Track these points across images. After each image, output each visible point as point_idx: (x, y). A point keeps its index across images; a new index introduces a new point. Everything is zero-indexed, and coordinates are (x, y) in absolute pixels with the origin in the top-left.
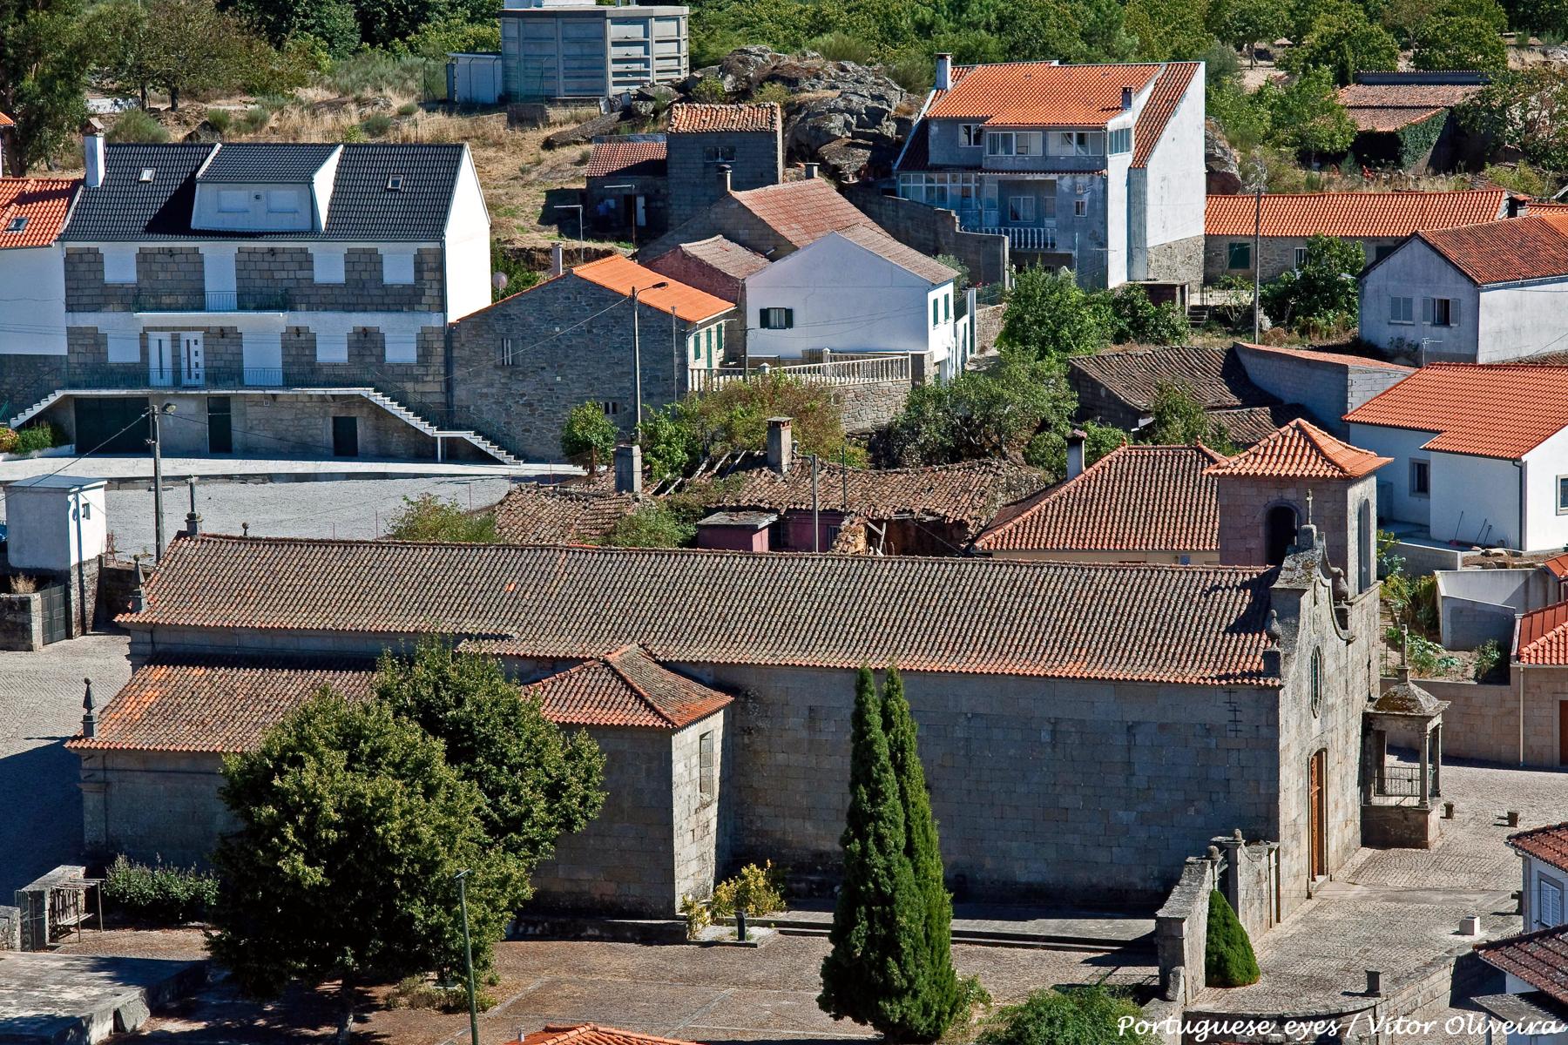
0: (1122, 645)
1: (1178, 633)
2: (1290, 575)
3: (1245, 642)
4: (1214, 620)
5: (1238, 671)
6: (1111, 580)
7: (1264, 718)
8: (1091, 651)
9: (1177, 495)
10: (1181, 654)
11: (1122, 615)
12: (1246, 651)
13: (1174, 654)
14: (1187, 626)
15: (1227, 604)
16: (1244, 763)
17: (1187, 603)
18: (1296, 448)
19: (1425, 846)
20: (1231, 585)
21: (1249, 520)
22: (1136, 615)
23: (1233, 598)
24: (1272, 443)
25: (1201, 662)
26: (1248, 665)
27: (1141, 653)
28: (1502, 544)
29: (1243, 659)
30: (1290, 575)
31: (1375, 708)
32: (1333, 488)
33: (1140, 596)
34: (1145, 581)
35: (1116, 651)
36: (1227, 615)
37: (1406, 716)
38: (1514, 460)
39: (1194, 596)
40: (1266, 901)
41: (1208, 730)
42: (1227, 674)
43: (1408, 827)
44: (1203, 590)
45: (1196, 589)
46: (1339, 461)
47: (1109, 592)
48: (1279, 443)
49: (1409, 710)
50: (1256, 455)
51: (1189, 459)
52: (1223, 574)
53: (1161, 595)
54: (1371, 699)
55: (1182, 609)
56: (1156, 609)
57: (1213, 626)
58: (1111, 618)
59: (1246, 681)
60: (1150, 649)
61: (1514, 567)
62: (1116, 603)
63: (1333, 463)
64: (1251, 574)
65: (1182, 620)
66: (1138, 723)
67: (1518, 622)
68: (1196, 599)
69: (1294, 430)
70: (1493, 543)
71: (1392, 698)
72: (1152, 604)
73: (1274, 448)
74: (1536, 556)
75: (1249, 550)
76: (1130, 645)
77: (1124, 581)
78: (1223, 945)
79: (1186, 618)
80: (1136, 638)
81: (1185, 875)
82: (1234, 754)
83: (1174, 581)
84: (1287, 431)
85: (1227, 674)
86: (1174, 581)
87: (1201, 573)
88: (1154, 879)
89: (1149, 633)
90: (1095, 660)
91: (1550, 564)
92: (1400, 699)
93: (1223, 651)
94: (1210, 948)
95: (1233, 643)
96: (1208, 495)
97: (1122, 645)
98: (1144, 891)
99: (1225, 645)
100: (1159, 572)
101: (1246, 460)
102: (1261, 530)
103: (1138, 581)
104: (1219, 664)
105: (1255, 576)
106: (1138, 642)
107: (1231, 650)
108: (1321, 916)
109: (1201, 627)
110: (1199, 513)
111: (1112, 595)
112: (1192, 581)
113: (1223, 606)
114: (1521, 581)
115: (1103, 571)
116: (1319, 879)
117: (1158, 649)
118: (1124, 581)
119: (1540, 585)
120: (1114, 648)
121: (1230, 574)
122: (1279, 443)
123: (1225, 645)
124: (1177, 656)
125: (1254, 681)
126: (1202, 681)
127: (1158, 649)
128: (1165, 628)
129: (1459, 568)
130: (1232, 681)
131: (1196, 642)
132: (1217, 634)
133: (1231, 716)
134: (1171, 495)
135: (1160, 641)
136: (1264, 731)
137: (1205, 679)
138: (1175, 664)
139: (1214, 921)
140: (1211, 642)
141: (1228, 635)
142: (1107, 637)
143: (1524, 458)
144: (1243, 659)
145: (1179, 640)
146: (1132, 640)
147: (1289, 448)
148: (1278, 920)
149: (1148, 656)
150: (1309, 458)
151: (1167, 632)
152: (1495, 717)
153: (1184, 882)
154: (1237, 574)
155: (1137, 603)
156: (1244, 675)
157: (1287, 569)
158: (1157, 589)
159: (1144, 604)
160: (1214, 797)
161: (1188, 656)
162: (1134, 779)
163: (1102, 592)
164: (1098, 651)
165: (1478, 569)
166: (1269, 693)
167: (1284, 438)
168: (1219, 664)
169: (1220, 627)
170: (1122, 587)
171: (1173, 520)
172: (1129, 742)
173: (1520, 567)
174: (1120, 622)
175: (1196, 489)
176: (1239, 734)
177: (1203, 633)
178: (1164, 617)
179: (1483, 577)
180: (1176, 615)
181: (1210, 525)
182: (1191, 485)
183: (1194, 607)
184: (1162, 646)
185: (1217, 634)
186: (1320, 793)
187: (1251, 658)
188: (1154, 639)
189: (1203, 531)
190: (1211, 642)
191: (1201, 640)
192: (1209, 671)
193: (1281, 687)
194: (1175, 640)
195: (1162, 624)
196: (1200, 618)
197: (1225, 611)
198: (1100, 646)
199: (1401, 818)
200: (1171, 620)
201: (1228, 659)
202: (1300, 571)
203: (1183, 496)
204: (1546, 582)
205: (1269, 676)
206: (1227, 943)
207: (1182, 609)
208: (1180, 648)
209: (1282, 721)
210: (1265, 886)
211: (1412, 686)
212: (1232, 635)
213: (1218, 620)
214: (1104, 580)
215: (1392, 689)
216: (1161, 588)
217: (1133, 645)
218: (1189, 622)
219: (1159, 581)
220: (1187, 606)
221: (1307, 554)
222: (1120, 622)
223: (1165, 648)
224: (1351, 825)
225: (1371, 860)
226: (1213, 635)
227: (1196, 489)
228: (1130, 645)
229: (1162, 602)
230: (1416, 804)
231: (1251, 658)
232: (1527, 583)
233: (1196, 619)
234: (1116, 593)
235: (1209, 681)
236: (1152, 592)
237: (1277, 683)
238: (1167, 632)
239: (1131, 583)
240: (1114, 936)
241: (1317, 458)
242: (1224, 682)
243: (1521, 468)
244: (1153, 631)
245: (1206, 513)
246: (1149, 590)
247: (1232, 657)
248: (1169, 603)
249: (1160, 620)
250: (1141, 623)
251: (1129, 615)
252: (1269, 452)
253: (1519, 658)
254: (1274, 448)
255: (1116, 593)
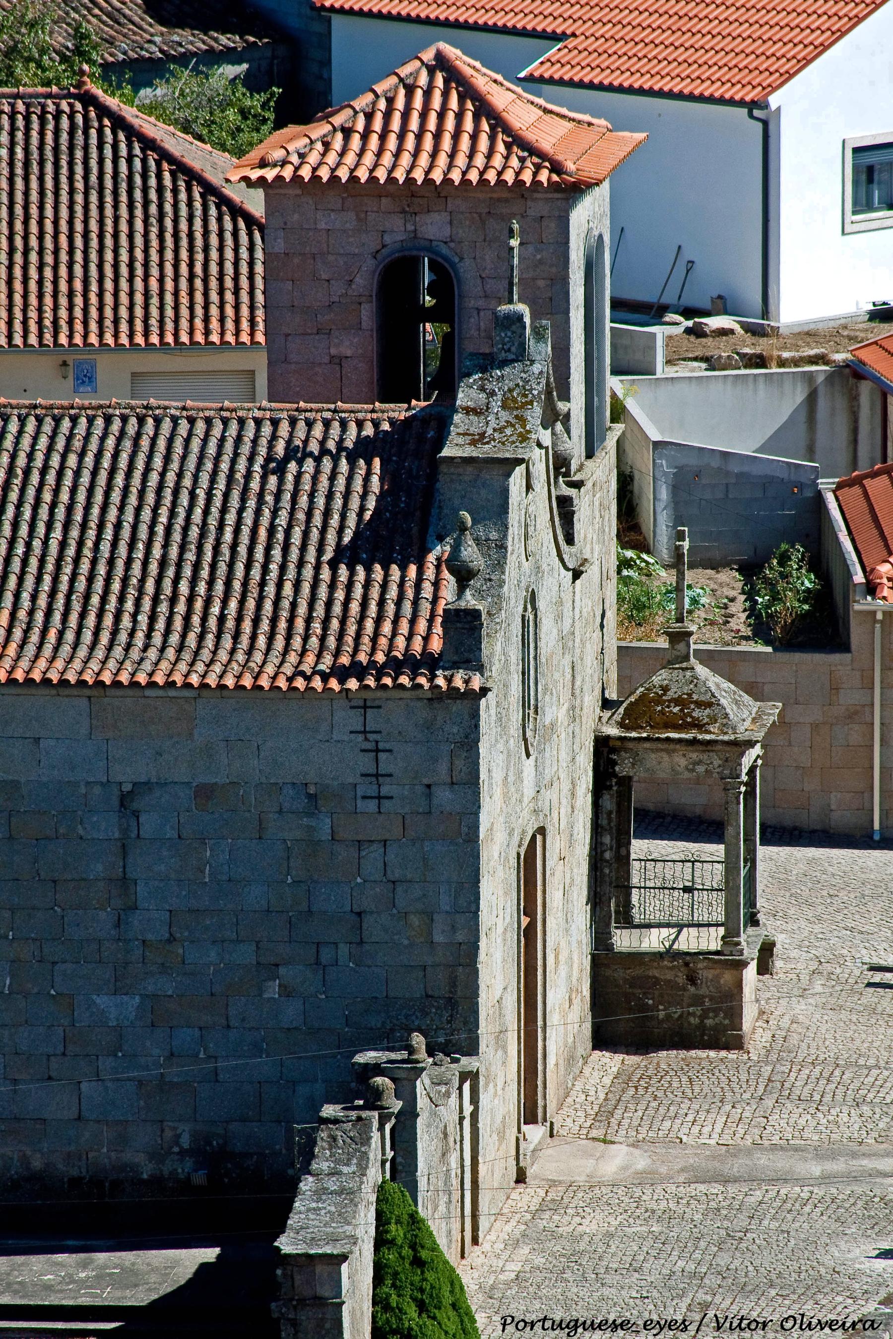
0: (95, 600)
1: (222, 568)
2: (475, 425)
3: (384, 587)
4: (306, 534)
5: (380, 658)
6: (43, 442)
7: (443, 768)
8: (22, 615)
9: (49, 212)
10: (239, 619)
11: (84, 526)
12: (391, 608)
13: (222, 619)
14: (242, 550)
15: (330, 496)
16: (396, 873)
17: (235, 495)
18: (441, 116)
19: (736, 1043)
20: (331, 445)
21: (338, 289)
22: (118, 526)
23: (341, 481)
24: (382, 105)
25: (289, 637)
26: (401, 642)
27: (143, 619)
28: (722, 305)
29: (387, 628)
30: (475, 425)
31: (621, 725)
32: (536, 208)
33: (119, 480)
34: (127, 444)
35: (83, 616)
36: (335, 521)
37: (694, 742)
38: (752, 105)
39: (248, 476)
40: (456, 1195)
41: (313, 798)
42: (355, 664)
43: (697, 1000)
44: (269, 459)
45: (251, 459)
46: (546, 145)
47: (44, 472)
48: (400, 103)
49: (698, 726)
50: (347, 132)
51: (65, 123)
52: (310, 424)
53: (171, 477)
54: (606, 704)
55: (224, 510)
56: (164, 512)
57: (303, 548)
58: (57, 534)
59: (404, 680)
60: (163, 608)
61: (782, 363)
62: (65, 497)
63: (533, 150)
64: (376, 424)
65: (228, 536)
66: (141, 788)
67: (830, 498)
68: (255, 485)
69: (431, 71)
70: (706, 304)
71: (658, 700)
72: (150, 498)
73: (388, 116)
74: (809, 335)
75: (338, 361)
76: (113, 600)
77: (77, 444)
78: (412, 1311)
79: (237, 532)
80: (125, 581)
81: (321, 1147)
82: (374, 853)
83: (196, 444)
84: (416, 74)
85: (355, 664)
86: (196, 444)
87: (258, 422)
88: (183, 1153)
89: (154, 568)
90: (35, 638)
91: (864, 355)
92: (677, 701)
93: (337, 609)
94: (382, 1318)
95: (358, 591)
96: (124, 211)
97: (95, 600)
98: (157, 1181)
99: (340, 595)
100: (158, 421)
101: (327, 145)
102: (367, 314)
103: (111, 442)
104: (332, 642)
105: (386, 426)
106: (132, 592)
107: (355, 607)
108: (566, 1224)
109: (277, 553)
110: (109, 256)
111: (51, 478)
112: (239, 440)
113: (320, 501)
114: (799, 396)
115: (22, 421)
116: (535, 1133)
117: (181, 608)
118: (77, 444)
119: (841, 403)
120: (76, 607)
121: (327, 424)
122: (400, 103)
123: (340, 595)
124: (230, 624)
125: (422, 680)
126: (300, 683)
127: (181, 608)
128: (190, 556)
129: (661, 370)
130: (371, 682)
131: (271, 590)
132: (317, 568)
133: (366, 763)
134: (34, 211)
135: (184, 588)
136: (443, 796)
137: (308, 679)
138: (227, 642)
139: (391, 1256)
140: (306, 588)
141: (343, 572)
142: (56, 580)
143: (774, 101)
144: (387, 628)
145: (228, 584)
146: (116, 586)
147: (424, 116)
148: (475, 1241)
149: (161, 625)
150: (474, 138)
151: (197, 567)
152: (815, 727)
153: (321, 1164)
154: (344, 424)
155: (116, 497)
156: (395, 665)
157: (468, 411)
158: (158, 462)
159: (133, 500)
160: (326, 955)
161: (256, 622)
162: (135, 920)
163: (27, 472)
164: (39, 616)
165: (699, 369)
166: (457, 707)
167: (410, 91)
168: (332, 642)
169: (320, 551)
170: (72, 460)
171: (48, 273)
172: (125, 831)
173: (796, 362)
174: (81, 544)
175: (94, 198)
176: (386, 803)
177: (283, 568)
178: (185, 529)
179: (716, 388)
180: (213, 522)
181: (139, 284)
182: (80, 185)
183: (252, 503)
184: (190, 600)
185: (317, 568)
186: (531, 927)
187: (404, 627)
188: (167, 584)
189: (124, 299)
190: (306, 588)
191: (280, 585)
192: (310, 659)
193: (484, 691)
194: (219, 587)
195: (183, 548)
196: (272, 531)
197: (327, 514)
198: (42, 601)
199: (681, 979)
200: (203, 535)
201: (352, 629)
202: (498, 416)
203: (64, 213)
204: (853, 398)
205: (456, 666)
206: (422, 1307)
207: (224, 510)
208: (233, 605)
209: (483, 775)
210: (453, 1159)
211: (702, 671)
212: (369, 570)
213: (315, 534)
214: (26, 442)
215: (656, 680)
216: (167, 459)
217: (122, 599)
218: (245, 539)
219: (162, 443)
220: (235, 501)
221: (512, 374)
222: (81, 544)
223: (199, 604)
224: (576, 1001)
225: (623, 1078)
226: (308, 572)
227: (94, 198)
228: (113, 600)
229: (176, 493)
230: (715, 945)
231: (404, 627)
232: (812, 399)
233: (263, 533)
234: (60, 474)
235: (317, 683)
236: (148, 469)
237: (476, 683)
238: (197, 567)
239: (93, 446)
240: (107, 1297)
241: (492, 138)
242: (353, 684)
243: (765, 123)
244: (163, 563)
245: (124, 257)
246: (140, 465)
247: (361, 622)
248: (193, 496)
249: (177, 537)
250: (132, 546)
251: (101, 527)
252: (377, 125)
253: (871, 588)
254: (388, 116)
255: (60, 474)
